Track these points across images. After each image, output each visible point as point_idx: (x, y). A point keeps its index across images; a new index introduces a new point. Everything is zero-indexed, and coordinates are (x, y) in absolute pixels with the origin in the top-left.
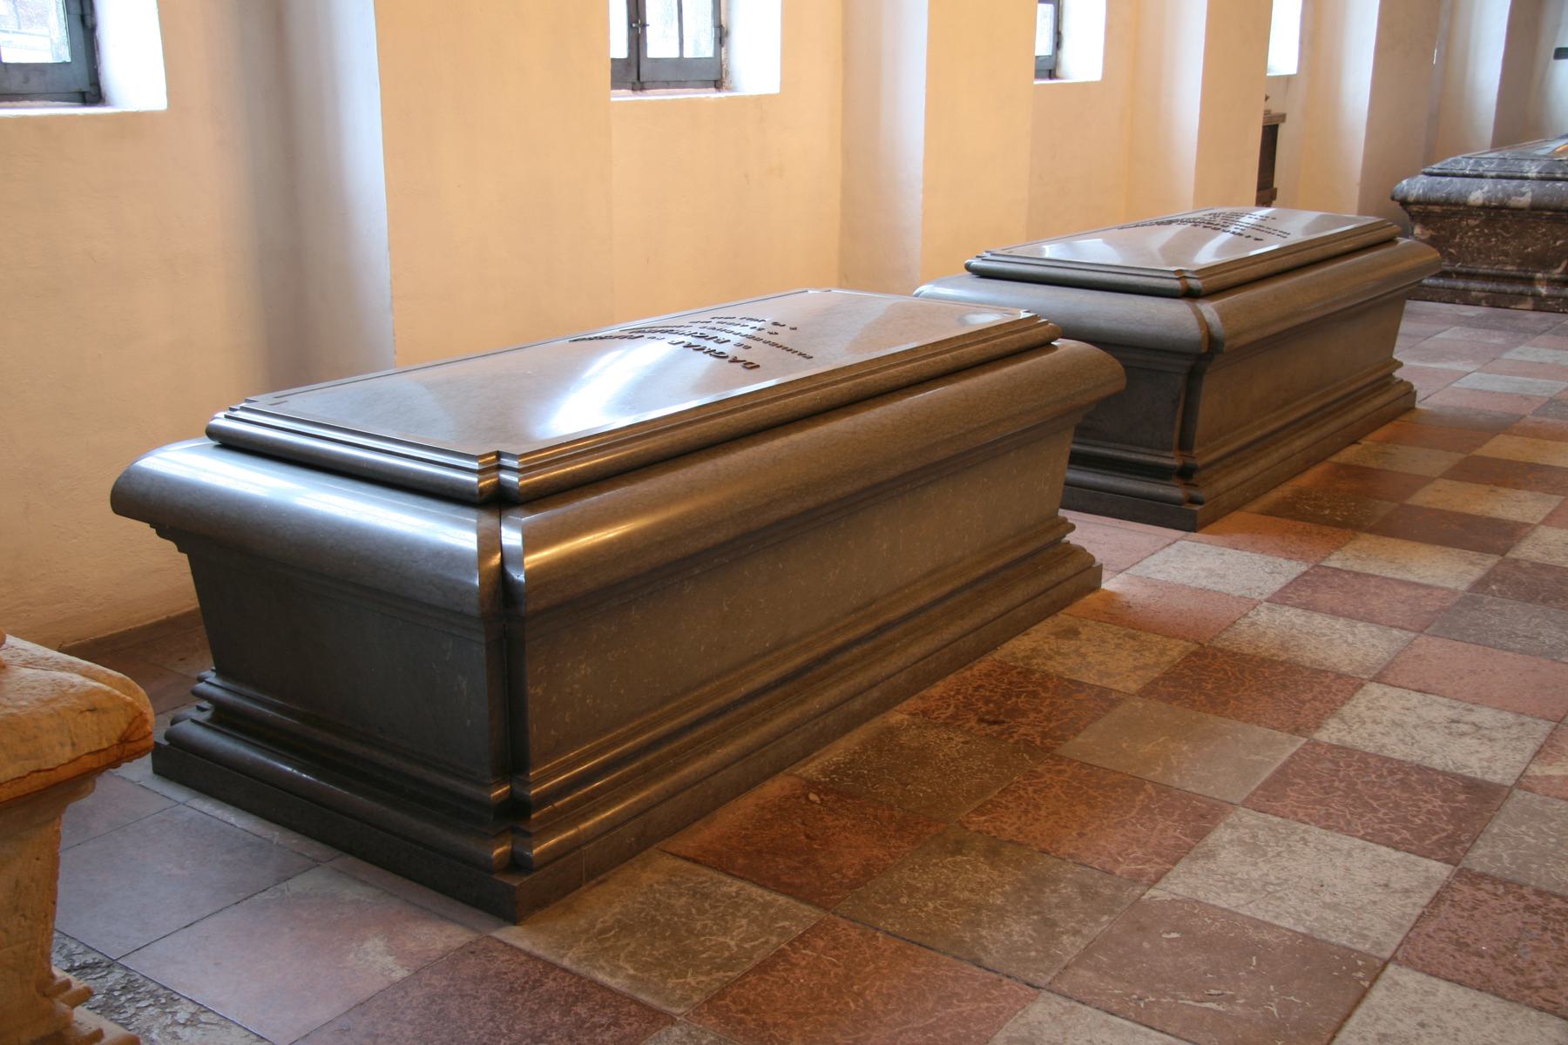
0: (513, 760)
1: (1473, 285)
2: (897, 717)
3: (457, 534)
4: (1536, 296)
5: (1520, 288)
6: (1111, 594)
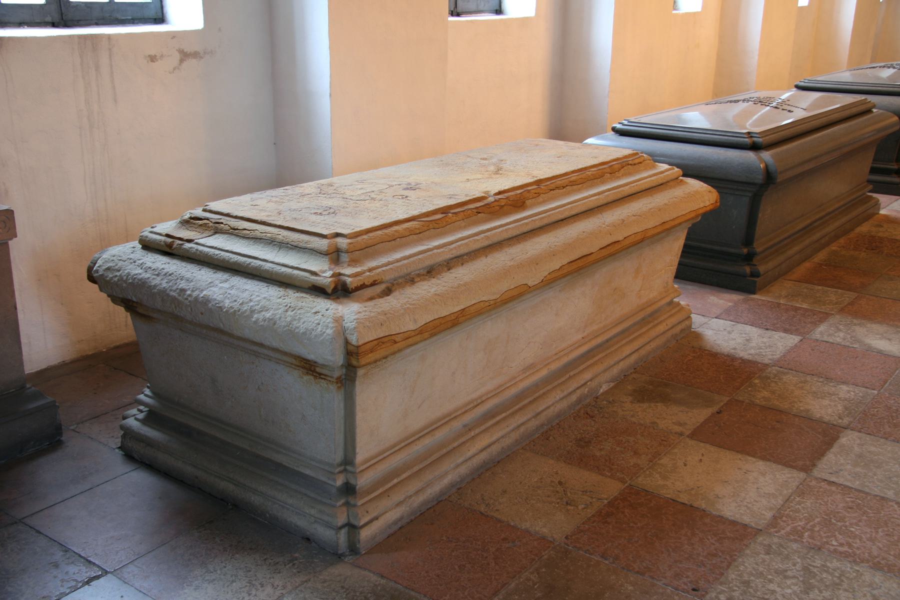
0: (748, 240)
2: (834, 247)
3: (750, 156)
6: (885, 216)
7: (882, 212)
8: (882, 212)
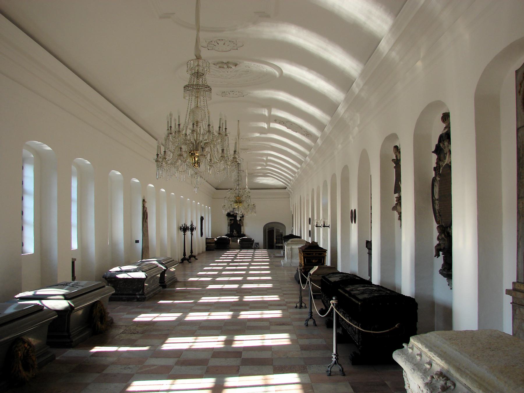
1: (123, 296)
4: (137, 298)
5: (133, 296)
7: (57, 358)
8: (57, 358)
